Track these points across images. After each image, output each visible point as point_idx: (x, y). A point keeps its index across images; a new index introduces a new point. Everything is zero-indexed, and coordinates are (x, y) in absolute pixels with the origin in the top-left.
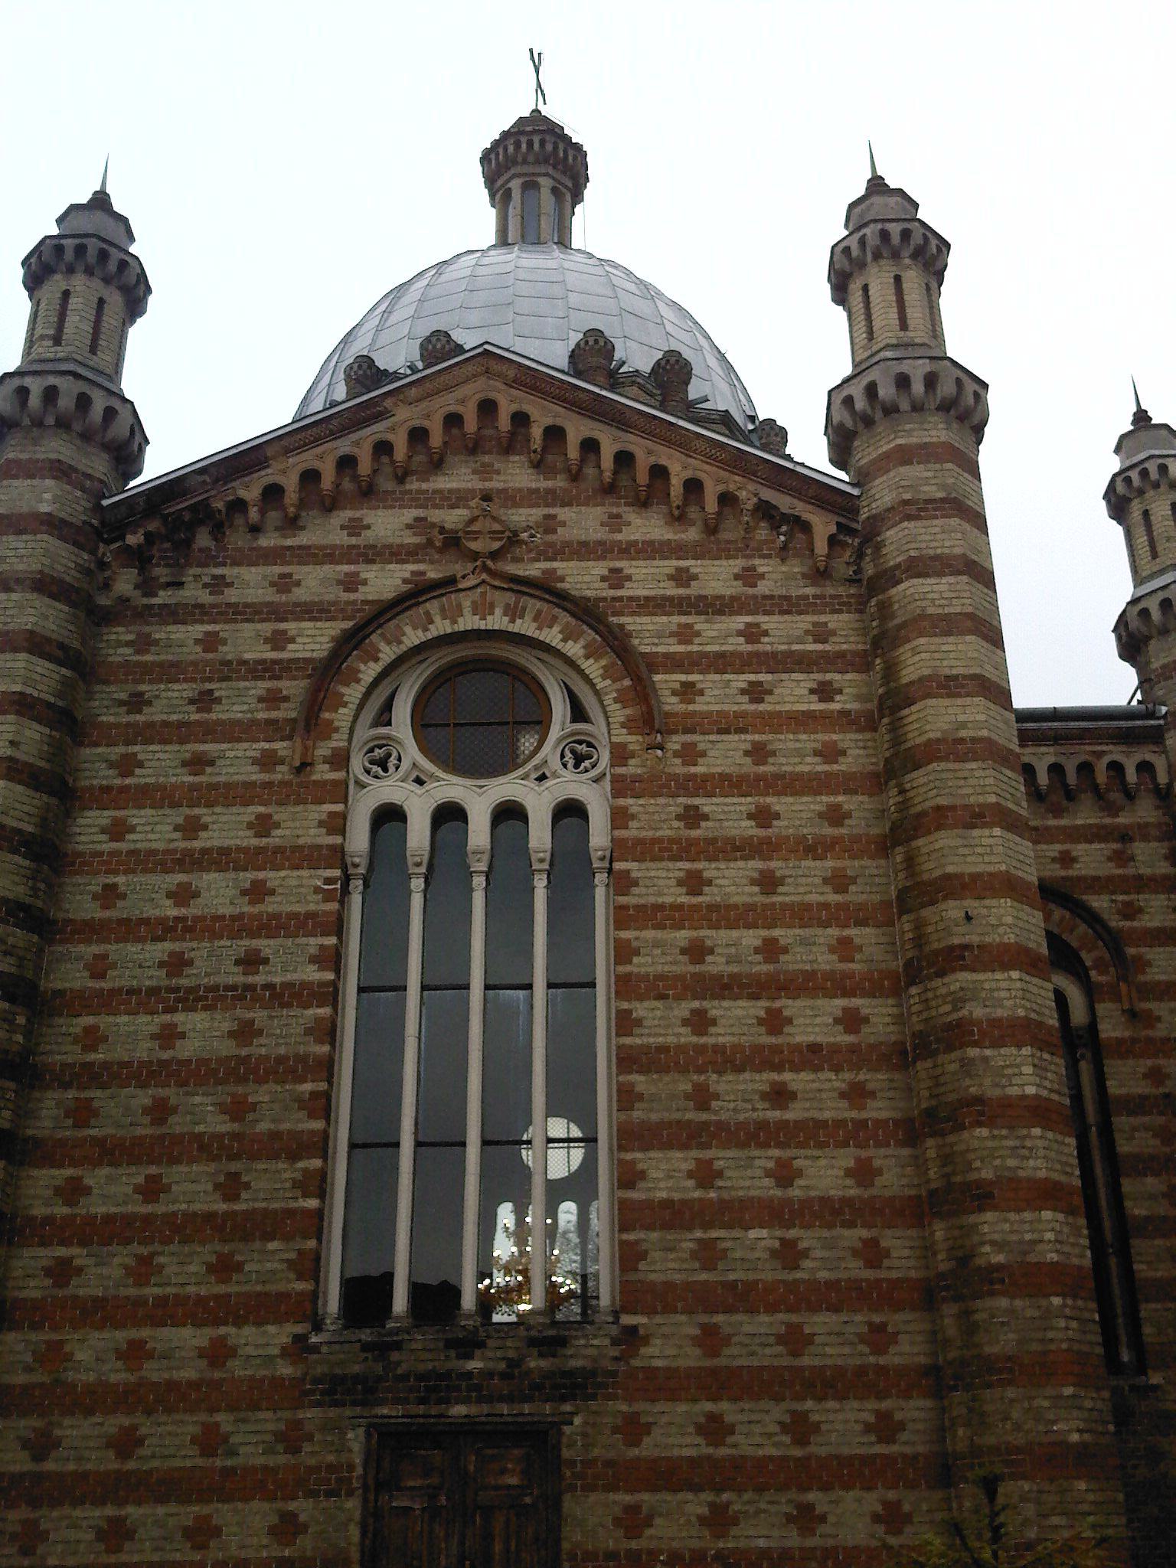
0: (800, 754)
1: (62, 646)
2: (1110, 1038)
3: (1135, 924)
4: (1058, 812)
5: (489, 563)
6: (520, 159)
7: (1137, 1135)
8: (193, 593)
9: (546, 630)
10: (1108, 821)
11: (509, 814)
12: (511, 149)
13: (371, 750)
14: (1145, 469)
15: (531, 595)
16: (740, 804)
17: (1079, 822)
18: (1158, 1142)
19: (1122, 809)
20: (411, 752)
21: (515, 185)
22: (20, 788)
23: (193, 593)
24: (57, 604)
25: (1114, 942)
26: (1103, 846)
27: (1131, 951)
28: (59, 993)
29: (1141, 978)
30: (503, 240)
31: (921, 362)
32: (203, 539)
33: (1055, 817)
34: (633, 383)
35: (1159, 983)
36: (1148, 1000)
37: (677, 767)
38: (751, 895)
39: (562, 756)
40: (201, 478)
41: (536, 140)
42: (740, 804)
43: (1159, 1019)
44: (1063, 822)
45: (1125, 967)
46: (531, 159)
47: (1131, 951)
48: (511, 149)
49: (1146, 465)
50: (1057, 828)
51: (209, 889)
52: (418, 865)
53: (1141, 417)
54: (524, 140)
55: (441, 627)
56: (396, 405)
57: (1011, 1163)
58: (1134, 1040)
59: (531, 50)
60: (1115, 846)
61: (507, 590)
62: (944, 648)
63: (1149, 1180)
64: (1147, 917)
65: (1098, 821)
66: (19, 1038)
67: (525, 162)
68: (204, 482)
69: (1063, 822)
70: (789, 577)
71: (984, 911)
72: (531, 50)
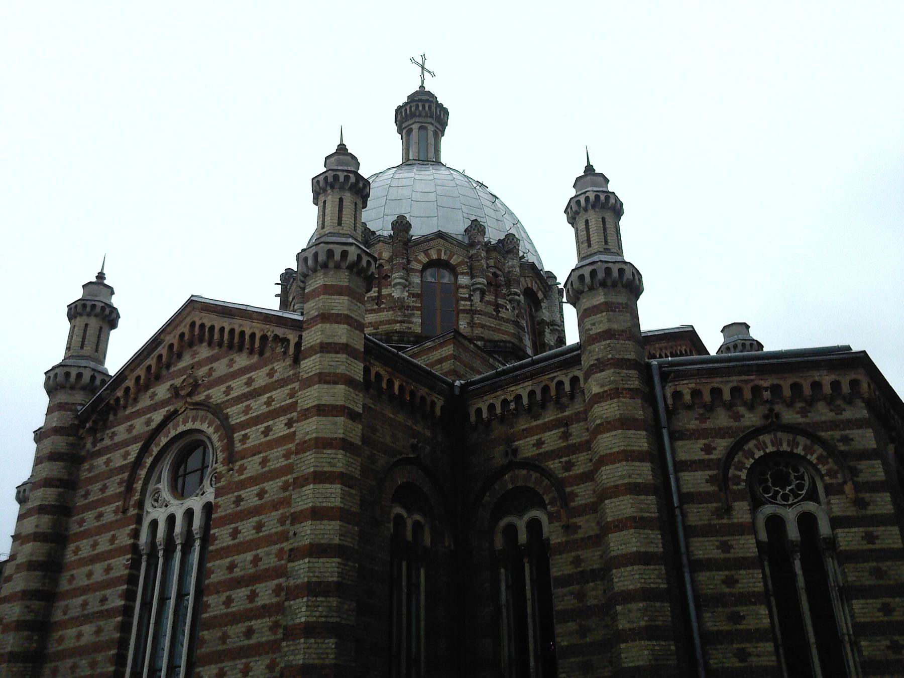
0: (277, 458)
1: (60, 480)
2: (555, 544)
3: (571, 473)
4: (536, 418)
5: (189, 400)
6: (417, 114)
7: (566, 598)
8: (107, 442)
9: (169, 435)
10: (560, 415)
11: (189, 513)
12: (413, 109)
13: (154, 495)
14: (599, 196)
15: (201, 410)
16: (255, 490)
17: (546, 420)
18: (575, 601)
19: (567, 406)
20: (166, 494)
21: (415, 127)
22: (39, 543)
23: (107, 442)
24: (57, 463)
25: (559, 485)
26: (557, 431)
27: (568, 489)
28: (56, 623)
29: (572, 504)
30: (407, 162)
31: (313, 248)
32: (111, 417)
33: (535, 420)
34: (379, 241)
35: (581, 505)
36: (575, 517)
37: (237, 478)
38: (253, 535)
39: (211, 480)
40: (106, 392)
41: (420, 104)
42: (255, 490)
43: (580, 527)
44: (539, 422)
45: (565, 499)
46: (423, 114)
47: (568, 489)
48: (413, 109)
49: (600, 194)
50: (537, 426)
51: (116, 569)
52: (160, 545)
53: (589, 169)
54: (420, 104)
55: (173, 433)
56: (165, 336)
57: (291, 658)
58: (567, 542)
59: (412, 60)
60: (562, 430)
61: (194, 409)
62: (307, 395)
63: (570, 624)
64: (576, 468)
65: (554, 417)
66: (35, 645)
67: (420, 116)
68: (108, 394)
69: (539, 422)
70: (285, 368)
71: (301, 529)
72: (412, 60)
